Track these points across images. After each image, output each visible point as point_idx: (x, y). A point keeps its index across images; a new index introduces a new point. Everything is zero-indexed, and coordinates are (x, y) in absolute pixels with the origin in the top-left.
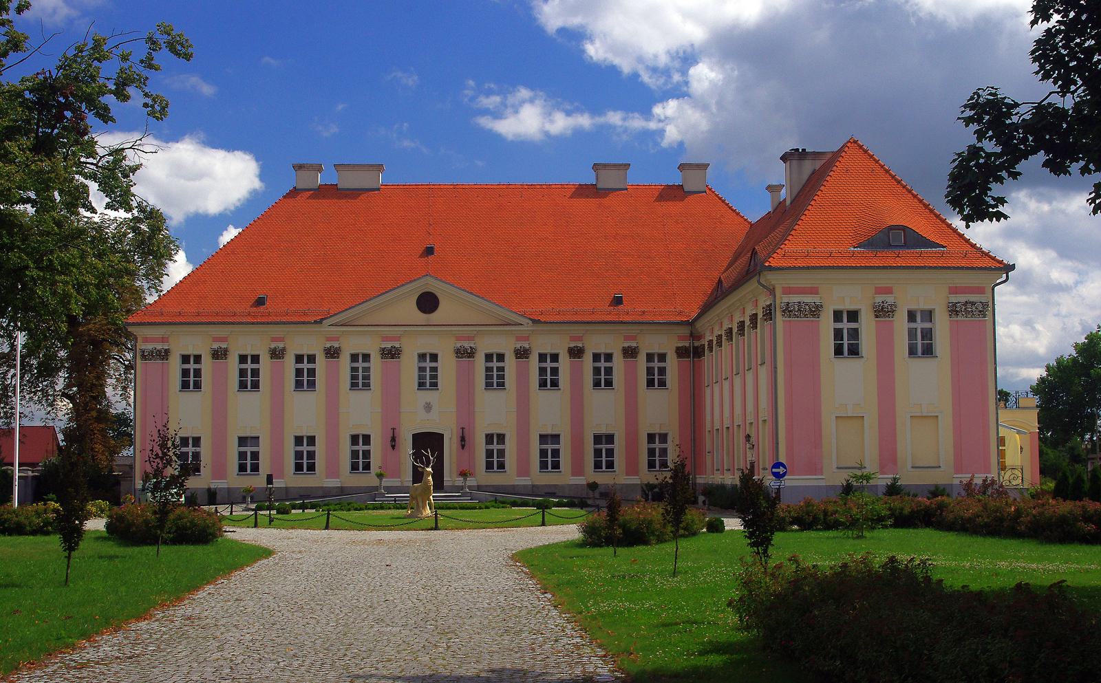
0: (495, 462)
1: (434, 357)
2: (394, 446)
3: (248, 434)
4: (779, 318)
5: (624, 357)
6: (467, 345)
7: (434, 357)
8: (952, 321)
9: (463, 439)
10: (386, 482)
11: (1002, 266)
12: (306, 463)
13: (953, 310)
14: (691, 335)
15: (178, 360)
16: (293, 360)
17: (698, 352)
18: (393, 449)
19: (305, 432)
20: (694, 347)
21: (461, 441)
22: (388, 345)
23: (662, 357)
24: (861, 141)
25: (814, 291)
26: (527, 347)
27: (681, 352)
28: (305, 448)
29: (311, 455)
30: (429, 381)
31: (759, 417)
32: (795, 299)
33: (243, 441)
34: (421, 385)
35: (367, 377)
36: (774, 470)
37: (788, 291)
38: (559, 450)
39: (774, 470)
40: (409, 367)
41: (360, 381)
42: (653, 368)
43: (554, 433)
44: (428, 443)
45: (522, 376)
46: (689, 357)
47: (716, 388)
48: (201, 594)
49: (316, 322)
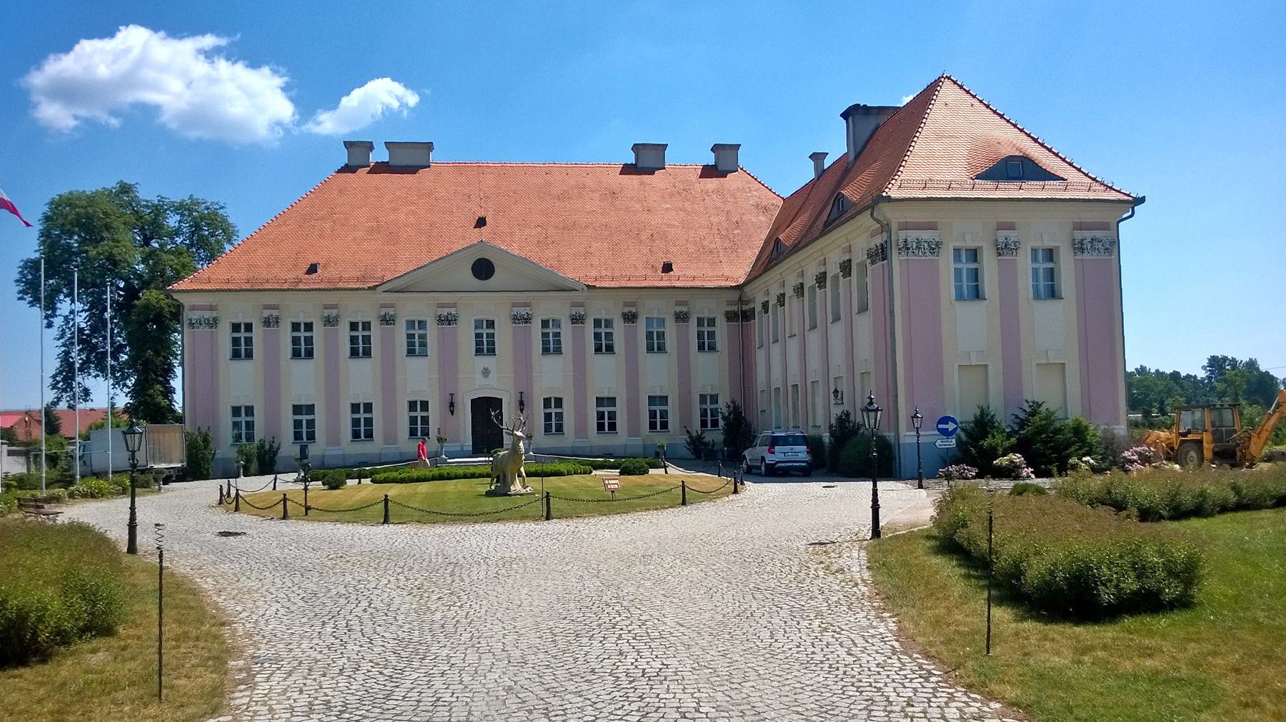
0: (554, 425)
1: (491, 324)
2: (453, 411)
3: (303, 402)
4: (896, 259)
5: (676, 322)
6: (523, 311)
7: (491, 324)
8: (1077, 259)
9: (521, 403)
10: (448, 447)
11: (1131, 199)
12: (363, 430)
13: (1079, 247)
14: (740, 299)
15: (228, 328)
16: (348, 327)
17: (747, 316)
18: (453, 414)
19: (361, 400)
20: (742, 311)
21: (450, 406)
22: (445, 312)
23: (712, 322)
24: (954, 77)
25: (932, 226)
26: (583, 313)
27: (730, 317)
28: (362, 416)
29: (369, 422)
30: (485, 346)
31: (788, 381)
32: (913, 235)
33: (297, 409)
34: (479, 351)
35: (423, 345)
36: (940, 426)
37: (905, 226)
38: (372, 418)
39: (940, 426)
40: (466, 335)
41: (415, 348)
42: (703, 332)
43: (611, 396)
44: (486, 409)
45: (332, 345)
46: (738, 321)
47: (776, 349)
48: (438, 403)
49: (370, 288)
